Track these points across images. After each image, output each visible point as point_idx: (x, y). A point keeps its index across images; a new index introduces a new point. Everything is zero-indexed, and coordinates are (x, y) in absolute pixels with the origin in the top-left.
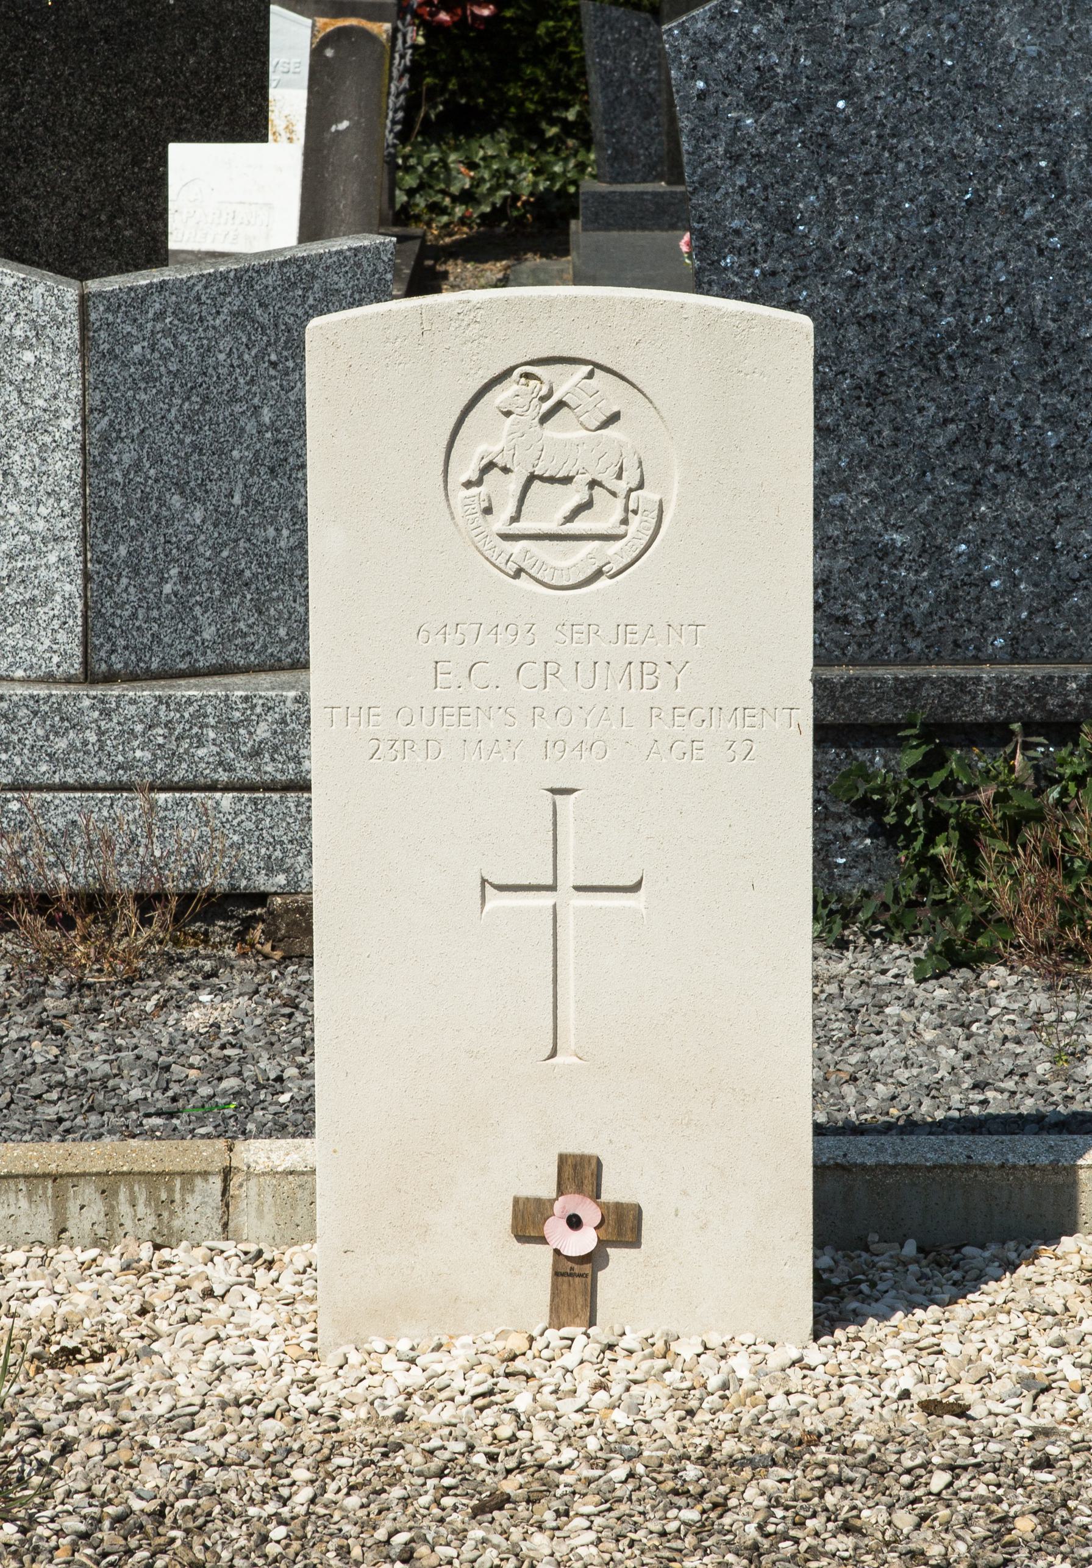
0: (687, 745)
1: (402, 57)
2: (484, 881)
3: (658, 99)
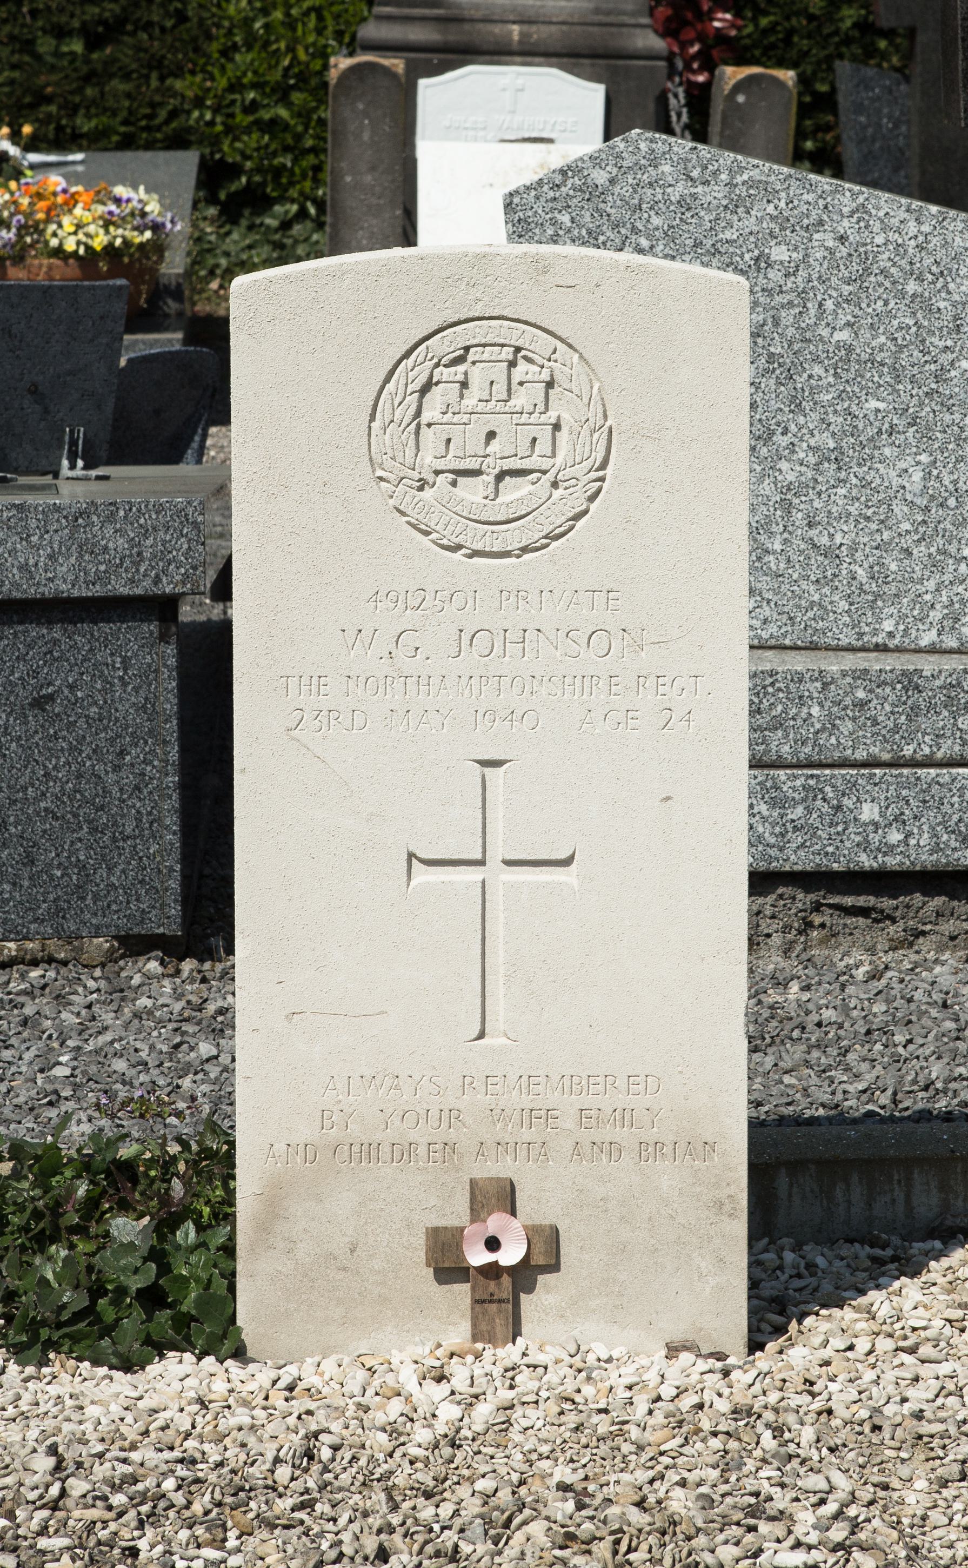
0: (621, 716)
1: (679, 115)
2: (411, 856)
3: (907, 154)
